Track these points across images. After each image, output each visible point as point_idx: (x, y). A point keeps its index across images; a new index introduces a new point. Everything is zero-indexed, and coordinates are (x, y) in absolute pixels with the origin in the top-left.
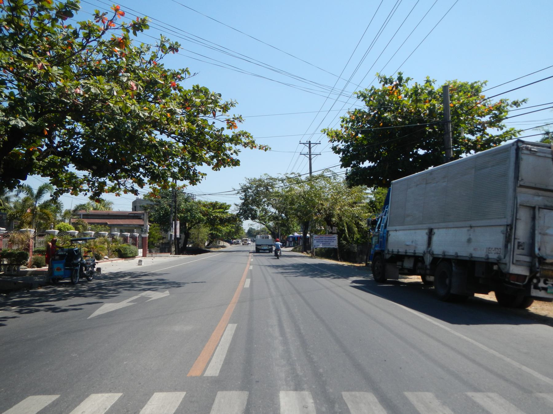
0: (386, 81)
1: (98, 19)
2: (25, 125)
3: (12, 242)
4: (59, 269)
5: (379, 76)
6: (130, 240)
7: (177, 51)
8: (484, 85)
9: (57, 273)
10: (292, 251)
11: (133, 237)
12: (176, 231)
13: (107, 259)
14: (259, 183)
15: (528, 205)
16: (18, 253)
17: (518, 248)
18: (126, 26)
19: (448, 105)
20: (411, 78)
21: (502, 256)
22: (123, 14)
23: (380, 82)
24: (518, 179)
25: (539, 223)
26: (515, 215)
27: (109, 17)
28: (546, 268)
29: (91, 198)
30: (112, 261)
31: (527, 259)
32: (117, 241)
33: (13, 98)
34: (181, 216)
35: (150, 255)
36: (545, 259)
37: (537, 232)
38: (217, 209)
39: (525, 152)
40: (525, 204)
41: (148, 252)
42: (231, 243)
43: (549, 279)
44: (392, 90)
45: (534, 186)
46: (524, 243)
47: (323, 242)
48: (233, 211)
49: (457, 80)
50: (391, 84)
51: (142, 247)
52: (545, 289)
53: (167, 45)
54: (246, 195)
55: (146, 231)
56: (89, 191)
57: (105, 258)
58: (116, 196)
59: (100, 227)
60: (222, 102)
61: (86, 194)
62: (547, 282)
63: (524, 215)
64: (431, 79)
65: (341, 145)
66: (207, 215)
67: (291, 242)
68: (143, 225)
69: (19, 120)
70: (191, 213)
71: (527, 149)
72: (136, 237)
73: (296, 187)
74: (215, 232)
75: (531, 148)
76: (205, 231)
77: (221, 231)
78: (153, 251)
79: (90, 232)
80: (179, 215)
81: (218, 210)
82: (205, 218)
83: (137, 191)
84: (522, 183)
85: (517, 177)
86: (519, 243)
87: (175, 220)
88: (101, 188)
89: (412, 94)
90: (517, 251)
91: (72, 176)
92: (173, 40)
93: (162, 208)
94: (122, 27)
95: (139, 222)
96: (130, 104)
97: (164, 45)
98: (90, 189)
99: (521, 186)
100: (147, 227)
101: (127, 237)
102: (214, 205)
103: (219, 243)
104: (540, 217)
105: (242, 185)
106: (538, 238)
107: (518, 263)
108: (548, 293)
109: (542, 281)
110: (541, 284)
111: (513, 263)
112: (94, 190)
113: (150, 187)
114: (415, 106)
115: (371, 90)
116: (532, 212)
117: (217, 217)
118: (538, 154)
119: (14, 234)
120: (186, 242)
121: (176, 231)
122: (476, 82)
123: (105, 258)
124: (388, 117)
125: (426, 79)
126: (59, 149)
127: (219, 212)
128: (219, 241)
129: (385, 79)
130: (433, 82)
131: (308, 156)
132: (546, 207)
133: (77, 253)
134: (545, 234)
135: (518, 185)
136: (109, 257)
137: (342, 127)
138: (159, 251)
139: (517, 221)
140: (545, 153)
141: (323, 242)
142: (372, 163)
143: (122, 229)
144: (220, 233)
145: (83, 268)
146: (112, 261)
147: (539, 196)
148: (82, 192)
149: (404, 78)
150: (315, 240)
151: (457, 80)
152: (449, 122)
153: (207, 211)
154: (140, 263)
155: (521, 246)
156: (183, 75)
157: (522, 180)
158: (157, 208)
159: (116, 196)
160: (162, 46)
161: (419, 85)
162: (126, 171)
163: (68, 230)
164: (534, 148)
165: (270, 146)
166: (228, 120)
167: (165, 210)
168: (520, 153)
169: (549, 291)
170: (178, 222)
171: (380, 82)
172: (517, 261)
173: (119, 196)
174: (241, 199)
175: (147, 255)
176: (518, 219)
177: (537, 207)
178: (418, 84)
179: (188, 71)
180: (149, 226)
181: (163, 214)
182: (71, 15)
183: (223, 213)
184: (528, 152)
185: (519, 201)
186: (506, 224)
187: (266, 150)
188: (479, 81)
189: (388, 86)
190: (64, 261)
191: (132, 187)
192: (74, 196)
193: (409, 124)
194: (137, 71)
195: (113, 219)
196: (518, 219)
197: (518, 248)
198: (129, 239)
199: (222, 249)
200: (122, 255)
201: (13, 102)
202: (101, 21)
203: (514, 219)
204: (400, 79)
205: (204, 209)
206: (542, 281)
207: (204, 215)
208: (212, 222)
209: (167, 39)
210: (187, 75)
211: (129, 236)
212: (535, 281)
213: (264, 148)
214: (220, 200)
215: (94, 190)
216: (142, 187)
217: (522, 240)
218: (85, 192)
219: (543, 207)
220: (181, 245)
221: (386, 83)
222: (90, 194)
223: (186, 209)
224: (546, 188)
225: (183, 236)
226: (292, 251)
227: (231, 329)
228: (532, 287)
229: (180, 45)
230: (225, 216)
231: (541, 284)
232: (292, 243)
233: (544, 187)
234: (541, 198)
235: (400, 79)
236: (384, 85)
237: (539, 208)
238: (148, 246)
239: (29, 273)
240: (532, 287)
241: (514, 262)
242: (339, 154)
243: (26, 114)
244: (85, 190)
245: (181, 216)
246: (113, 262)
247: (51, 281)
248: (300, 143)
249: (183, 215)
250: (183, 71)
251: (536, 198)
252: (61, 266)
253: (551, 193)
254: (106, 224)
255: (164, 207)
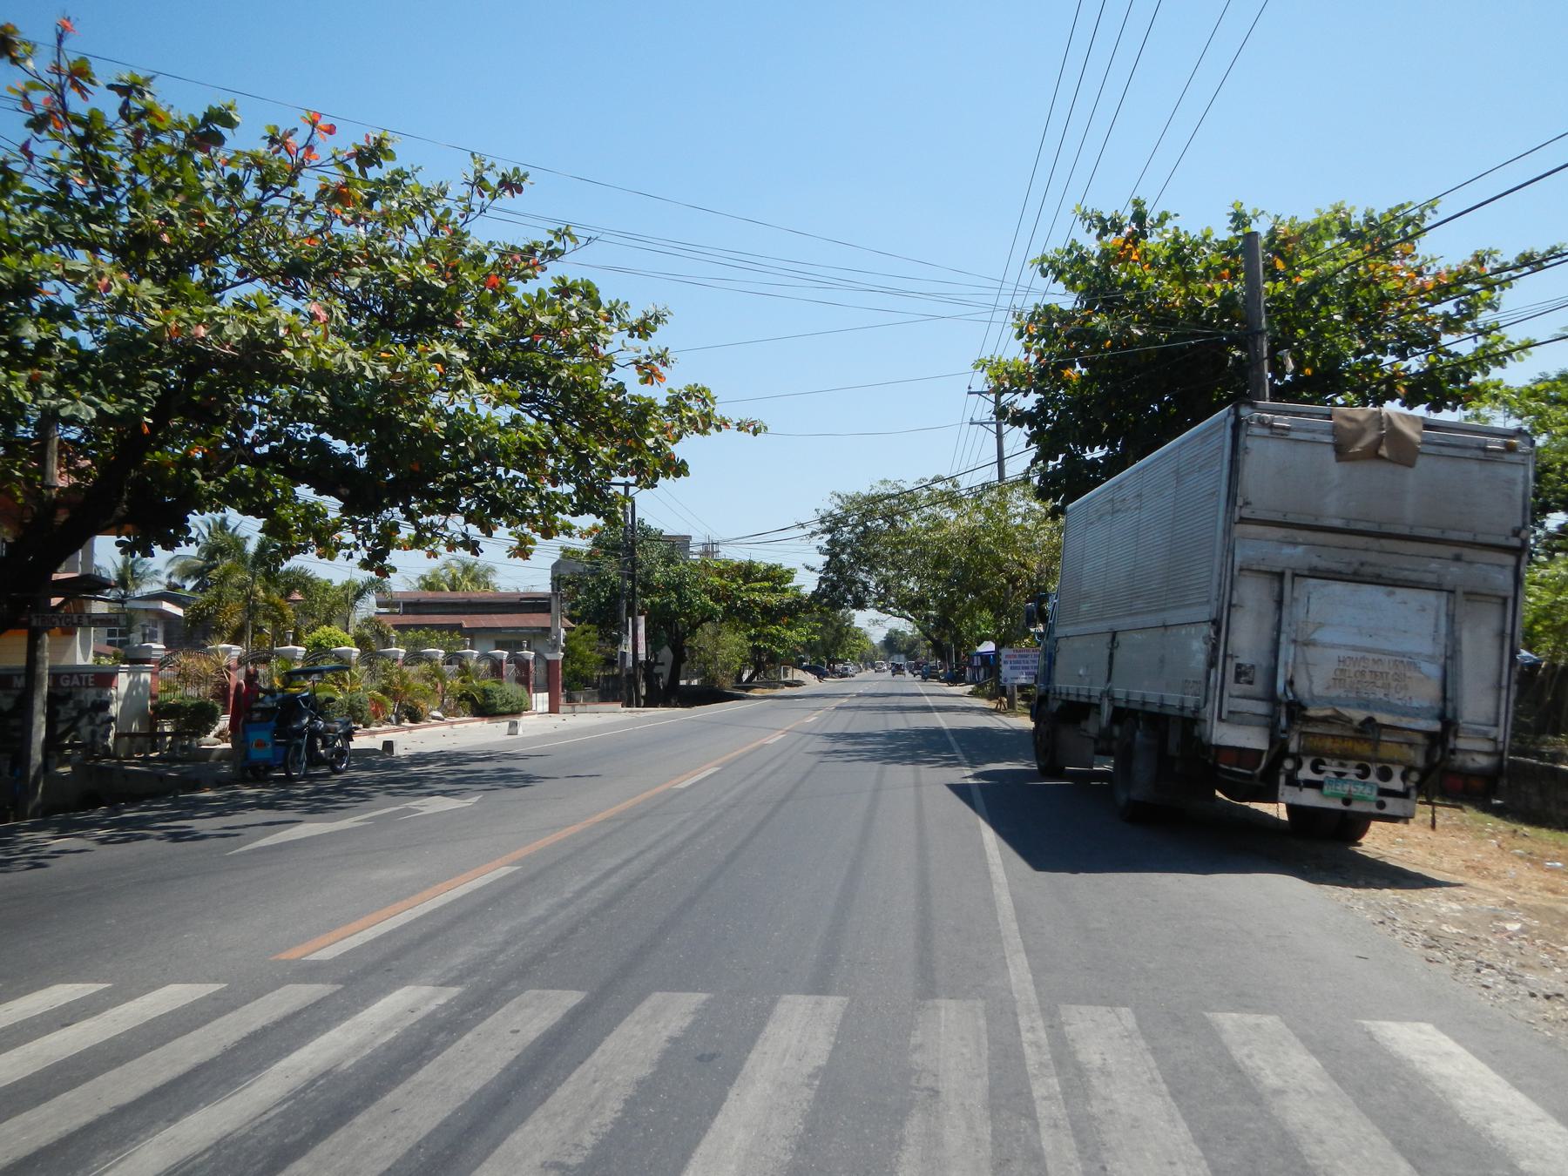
0: (1106, 226)
1: (276, 146)
2: (94, 414)
3: (184, 677)
4: (261, 744)
5: (1084, 216)
6: (509, 669)
7: (520, 190)
8: (1428, 212)
9: (257, 754)
10: (970, 693)
11: (523, 665)
12: (635, 643)
13: (438, 719)
14: (868, 506)
15: (1263, 568)
16: (192, 706)
17: (1237, 681)
18: (340, 158)
19: (1258, 287)
20: (1172, 214)
21: (1202, 705)
22: (331, 130)
23: (1089, 230)
24: (1235, 504)
25: (1295, 613)
26: (1227, 596)
27: (297, 141)
28: (1316, 730)
29: (365, 565)
30: (453, 723)
31: (1262, 708)
32: (467, 673)
33: (75, 352)
34: (652, 602)
35: (569, 708)
36: (1304, 708)
37: (1283, 638)
38: (757, 580)
39: (1257, 431)
40: (1255, 567)
41: (562, 700)
42: (821, 675)
43: (1327, 761)
44: (1123, 248)
45: (1278, 517)
46: (1253, 667)
47: (1027, 668)
48: (807, 583)
49: (1343, 202)
50: (1118, 233)
51: (549, 686)
52: (1317, 785)
53: (493, 180)
54: (832, 542)
55: (555, 646)
56: (357, 547)
57: (434, 718)
58: (429, 557)
59: (438, 635)
60: (634, 316)
61: (350, 556)
62: (1322, 767)
63: (1253, 594)
64: (1248, 210)
65: (1028, 402)
66: (729, 597)
67: (978, 668)
68: (548, 629)
69: (81, 404)
70: (680, 596)
71: (1261, 422)
72: (528, 661)
73: (950, 515)
74: (767, 645)
75: (1273, 420)
76: (731, 644)
77: (784, 640)
78: (577, 697)
79: (291, 647)
80: (647, 601)
81: (758, 585)
82: (719, 608)
83: (476, 543)
84: (1246, 513)
85: (1232, 497)
86: (1239, 666)
87: (631, 611)
88: (387, 540)
89: (1168, 259)
90: (1233, 688)
91: (312, 512)
92: (505, 167)
93: (604, 583)
94: (332, 161)
95: (537, 620)
96: (329, 352)
97: (483, 179)
98: (360, 542)
99: (1243, 520)
100: (558, 634)
101: (501, 661)
102: (747, 572)
103: (786, 675)
104: (1294, 600)
105: (822, 513)
106: (1287, 652)
107: (1235, 718)
108: (1327, 796)
109: (1307, 763)
110: (1306, 773)
111: (1220, 719)
112: (369, 544)
113: (511, 534)
114: (1182, 292)
115: (1070, 252)
116: (1276, 585)
117: (754, 601)
118: (1293, 435)
119: (189, 661)
120: (675, 675)
121: (635, 643)
122: (1402, 206)
123: (434, 718)
124: (1101, 327)
125: (1233, 210)
126: (257, 450)
127: (760, 590)
128: (785, 669)
129: (1101, 219)
130: (1254, 217)
131: (994, 427)
132: (1315, 573)
133: (306, 704)
134: (1309, 643)
135: (1237, 518)
136: (446, 715)
137: (1028, 350)
138: (596, 699)
139: (1233, 610)
140: (1313, 431)
141: (1027, 668)
142: (1102, 448)
143: (511, 641)
144: (780, 647)
145: (316, 742)
146: (453, 723)
147: (1295, 544)
148: (342, 551)
149: (1153, 215)
150: (1005, 662)
151: (1343, 202)
152: (1262, 333)
153: (724, 587)
154: (513, 730)
155: (1246, 674)
156: (558, 245)
157: (1247, 503)
158: (592, 581)
159: (429, 557)
160: (480, 183)
161: (1186, 232)
162: (433, 495)
163: (338, 645)
164: (1281, 421)
165: (766, 423)
166: (636, 362)
167: (613, 588)
168: (1242, 435)
169: (1327, 789)
170: (642, 618)
171: (1089, 230)
172: (1230, 712)
173: (436, 557)
174: (821, 551)
175: (561, 708)
176: (1235, 606)
177: (1288, 574)
178: (1182, 231)
179: (569, 235)
180: (563, 631)
181: (608, 599)
182: (219, 140)
183: (774, 590)
184: (1266, 432)
185: (1238, 559)
186: (1207, 618)
187: (755, 433)
188: (1410, 203)
189: (1111, 239)
190: (273, 724)
191: (463, 535)
192: (325, 560)
193: (1167, 342)
194: (386, 261)
195: (472, 613)
196: (1235, 606)
197: (1237, 681)
198: (505, 665)
199: (787, 691)
200: (483, 708)
201: (74, 361)
202: (283, 151)
203: (1226, 606)
204: (1139, 217)
205: (716, 581)
206: (1307, 763)
207: (717, 600)
208: (739, 614)
209: (487, 165)
210: (570, 245)
211: (505, 657)
212: (1289, 764)
213: (751, 428)
214: (764, 557)
215: (369, 544)
216: (490, 535)
217: (1245, 659)
218: (347, 552)
219: (1306, 573)
220: (662, 682)
221: (1104, 231)
222: (363, 553)
223: (667, 584)
224: (1319, 523)
225: (666, 654)
226: (972, 694)
227: (504, 871)
228: (1282, 779)
229: (526, 175)
230: (774, 600)
231: (1306, 773)
232: (982, 672)
233: (1310, 521)
234: (1300, 549)
235: (1139, 217)
236: (1099, 237)
237: (1295, 575)
238: (564, 686)
239: (215, 754)
240: (1282, 779)
241: (1224, 717)
242: (1021, 426)
243: (99, 388)
244: (348, 547)
245: (652, 602)
246: (455, 726)
247: (249, 774)
248: (970, 393)
249: (658, 600)
250: (559, 234)
251: (1287, 550)
252: (265, 736)
253: (1392, 531)
254: (459, 627)
255: (609, 579)
